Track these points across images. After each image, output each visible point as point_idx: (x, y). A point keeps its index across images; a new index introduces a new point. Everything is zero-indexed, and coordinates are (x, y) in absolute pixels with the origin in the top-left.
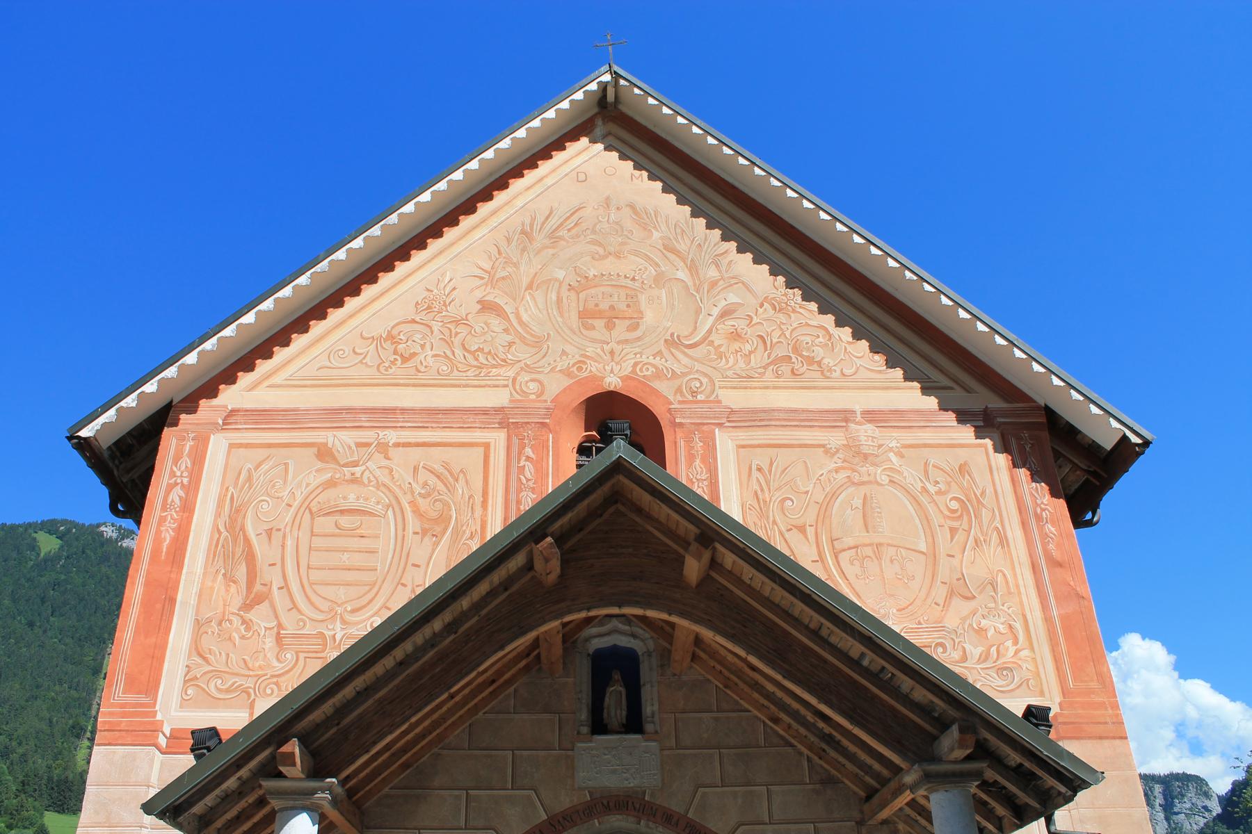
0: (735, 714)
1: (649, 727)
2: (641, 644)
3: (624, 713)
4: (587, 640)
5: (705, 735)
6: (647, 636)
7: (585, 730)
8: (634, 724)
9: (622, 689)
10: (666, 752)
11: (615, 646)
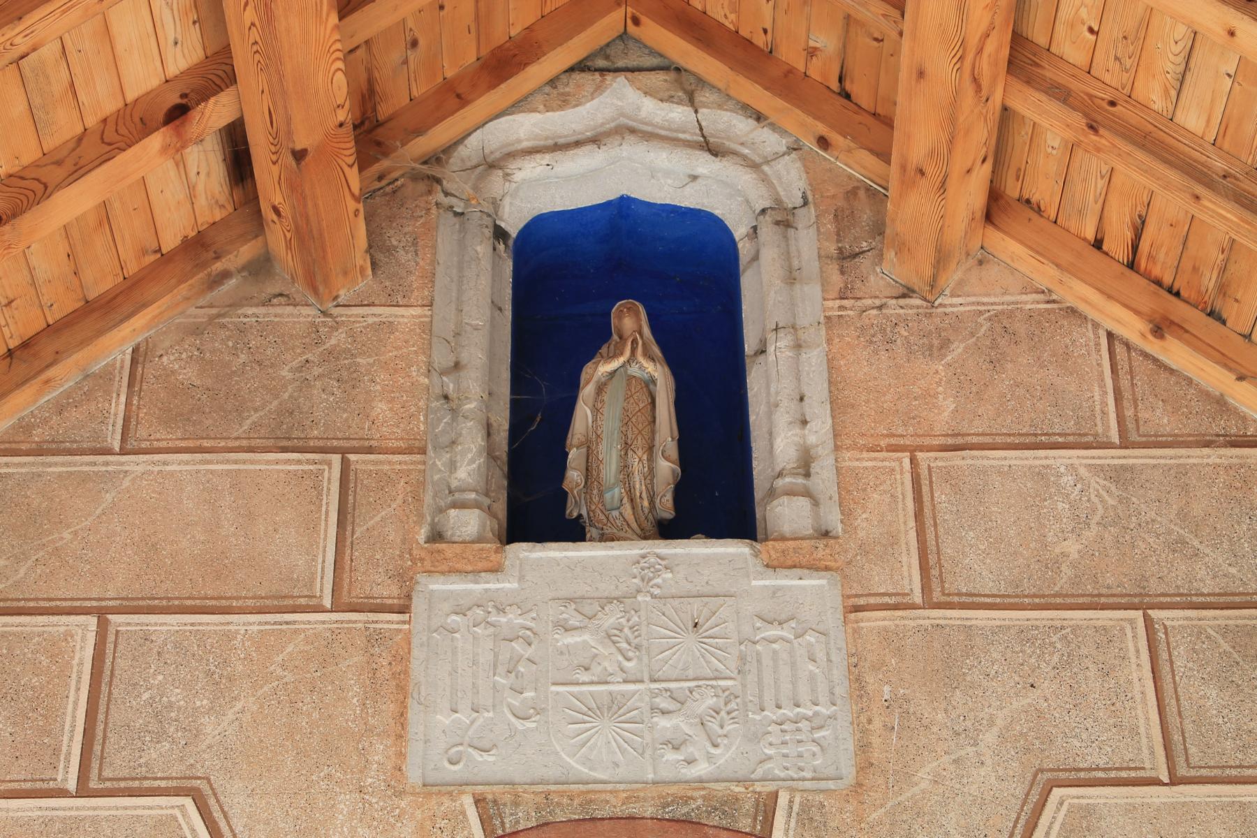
0: (1213, 456)
1: (784, 514)
2: (744, 179)
3: (667, 468)
4: (492, 164)
5: (1072, 547)
6: (770, 141)
7: (468, 523)
8: (715, 494)
9: (657, 372)
10: (874, 621)
11: (623, 207)
